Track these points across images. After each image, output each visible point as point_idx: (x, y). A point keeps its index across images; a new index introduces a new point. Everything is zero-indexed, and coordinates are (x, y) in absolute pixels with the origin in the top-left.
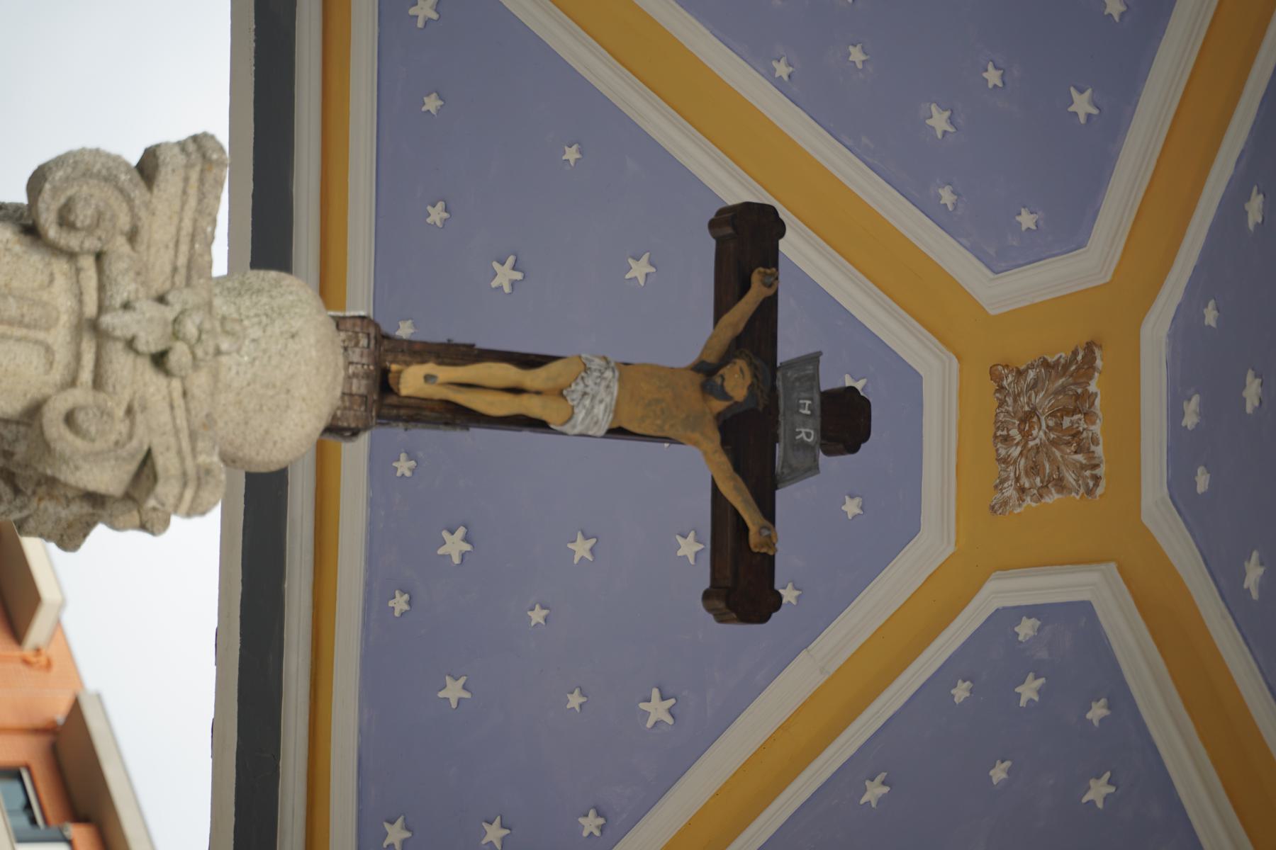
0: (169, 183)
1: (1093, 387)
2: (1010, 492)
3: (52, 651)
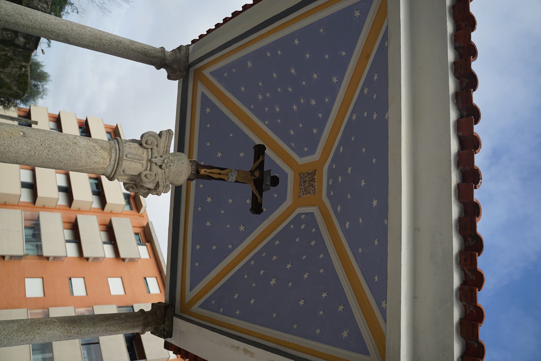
0: (164, 137)
1: (315, 177)
2: (301, 194)
3: (144, 214)
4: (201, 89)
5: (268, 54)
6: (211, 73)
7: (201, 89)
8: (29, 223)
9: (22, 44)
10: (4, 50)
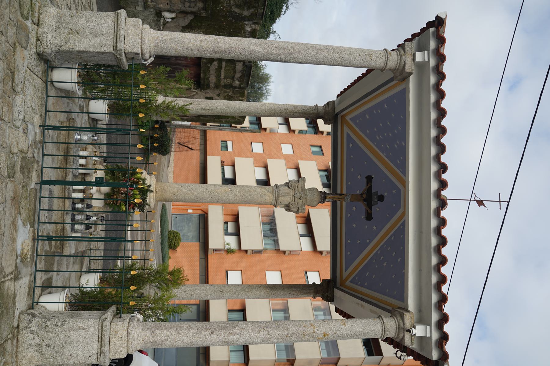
4: (346, 130)
6: (350, 119)
8: (266, 219)
9: (238, 86)
10: (226, 92)
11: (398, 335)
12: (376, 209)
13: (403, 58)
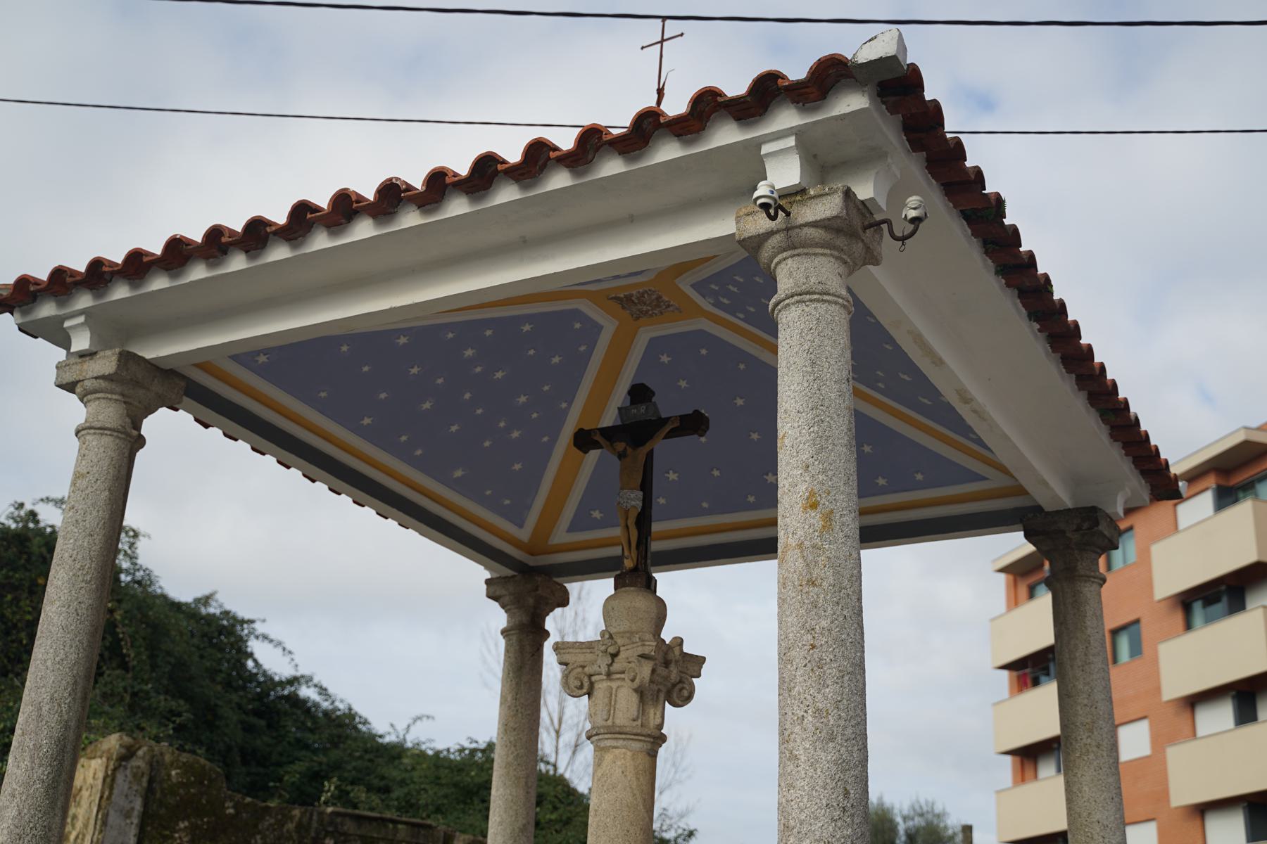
0: (567, 658)
4: (561, 536)
5: (419, 452)
7: (561, 536)
11: (817, 245)
12: (668, 405)
13: (88, 384)
